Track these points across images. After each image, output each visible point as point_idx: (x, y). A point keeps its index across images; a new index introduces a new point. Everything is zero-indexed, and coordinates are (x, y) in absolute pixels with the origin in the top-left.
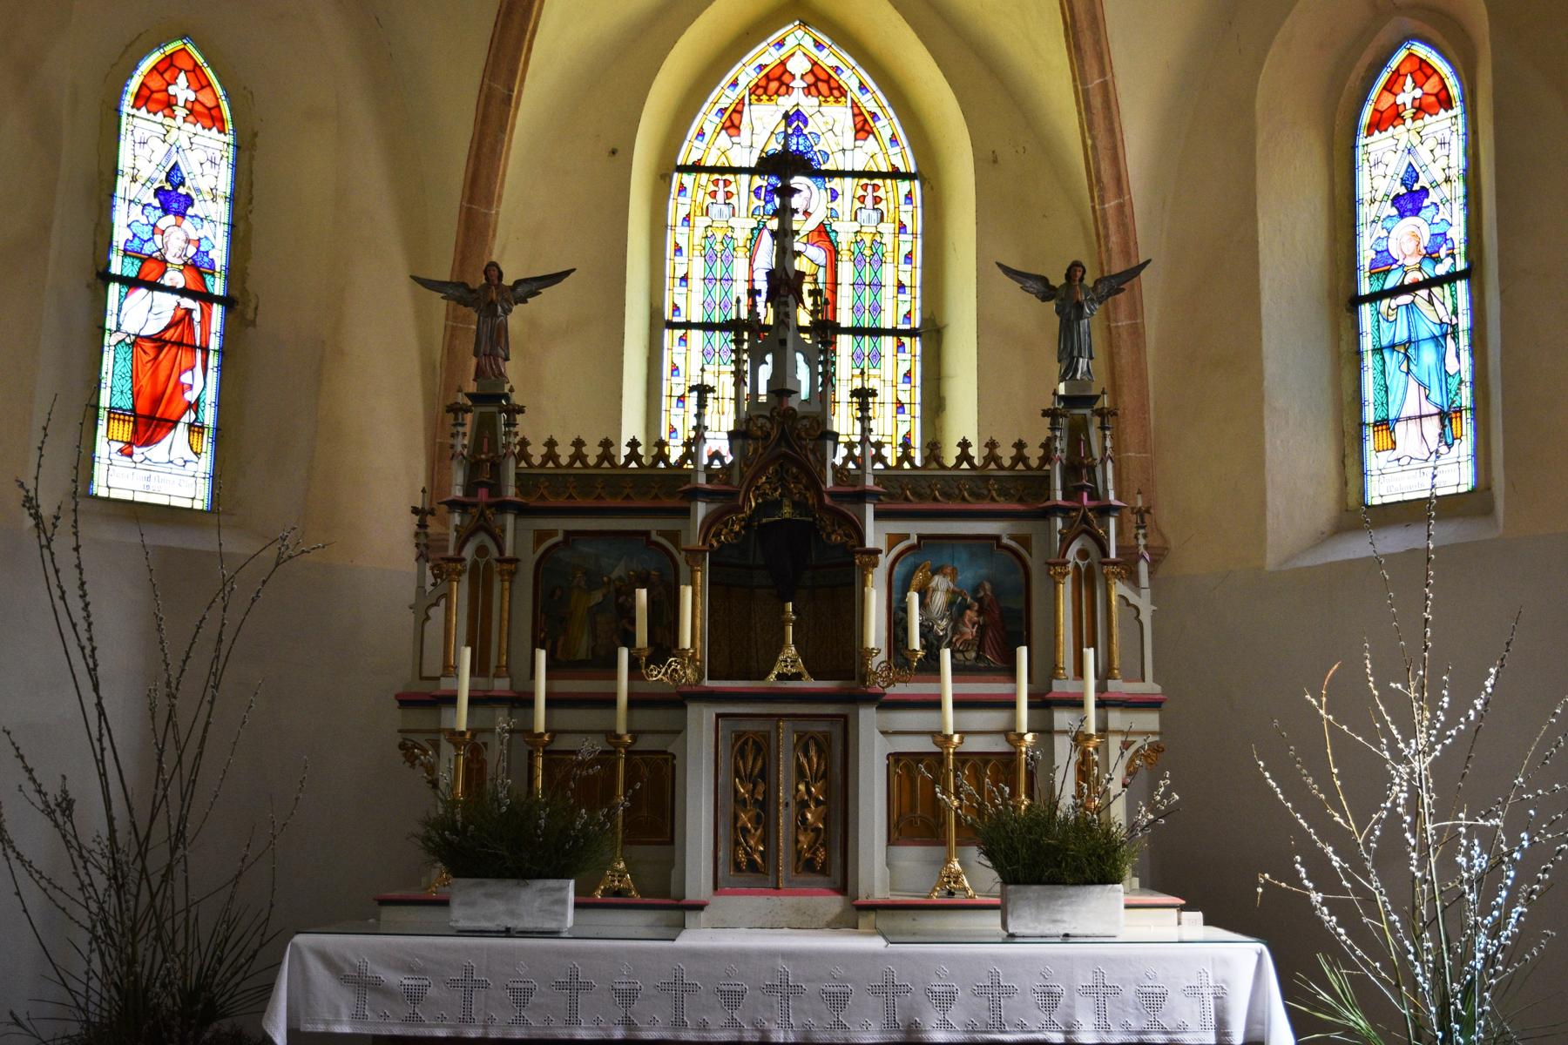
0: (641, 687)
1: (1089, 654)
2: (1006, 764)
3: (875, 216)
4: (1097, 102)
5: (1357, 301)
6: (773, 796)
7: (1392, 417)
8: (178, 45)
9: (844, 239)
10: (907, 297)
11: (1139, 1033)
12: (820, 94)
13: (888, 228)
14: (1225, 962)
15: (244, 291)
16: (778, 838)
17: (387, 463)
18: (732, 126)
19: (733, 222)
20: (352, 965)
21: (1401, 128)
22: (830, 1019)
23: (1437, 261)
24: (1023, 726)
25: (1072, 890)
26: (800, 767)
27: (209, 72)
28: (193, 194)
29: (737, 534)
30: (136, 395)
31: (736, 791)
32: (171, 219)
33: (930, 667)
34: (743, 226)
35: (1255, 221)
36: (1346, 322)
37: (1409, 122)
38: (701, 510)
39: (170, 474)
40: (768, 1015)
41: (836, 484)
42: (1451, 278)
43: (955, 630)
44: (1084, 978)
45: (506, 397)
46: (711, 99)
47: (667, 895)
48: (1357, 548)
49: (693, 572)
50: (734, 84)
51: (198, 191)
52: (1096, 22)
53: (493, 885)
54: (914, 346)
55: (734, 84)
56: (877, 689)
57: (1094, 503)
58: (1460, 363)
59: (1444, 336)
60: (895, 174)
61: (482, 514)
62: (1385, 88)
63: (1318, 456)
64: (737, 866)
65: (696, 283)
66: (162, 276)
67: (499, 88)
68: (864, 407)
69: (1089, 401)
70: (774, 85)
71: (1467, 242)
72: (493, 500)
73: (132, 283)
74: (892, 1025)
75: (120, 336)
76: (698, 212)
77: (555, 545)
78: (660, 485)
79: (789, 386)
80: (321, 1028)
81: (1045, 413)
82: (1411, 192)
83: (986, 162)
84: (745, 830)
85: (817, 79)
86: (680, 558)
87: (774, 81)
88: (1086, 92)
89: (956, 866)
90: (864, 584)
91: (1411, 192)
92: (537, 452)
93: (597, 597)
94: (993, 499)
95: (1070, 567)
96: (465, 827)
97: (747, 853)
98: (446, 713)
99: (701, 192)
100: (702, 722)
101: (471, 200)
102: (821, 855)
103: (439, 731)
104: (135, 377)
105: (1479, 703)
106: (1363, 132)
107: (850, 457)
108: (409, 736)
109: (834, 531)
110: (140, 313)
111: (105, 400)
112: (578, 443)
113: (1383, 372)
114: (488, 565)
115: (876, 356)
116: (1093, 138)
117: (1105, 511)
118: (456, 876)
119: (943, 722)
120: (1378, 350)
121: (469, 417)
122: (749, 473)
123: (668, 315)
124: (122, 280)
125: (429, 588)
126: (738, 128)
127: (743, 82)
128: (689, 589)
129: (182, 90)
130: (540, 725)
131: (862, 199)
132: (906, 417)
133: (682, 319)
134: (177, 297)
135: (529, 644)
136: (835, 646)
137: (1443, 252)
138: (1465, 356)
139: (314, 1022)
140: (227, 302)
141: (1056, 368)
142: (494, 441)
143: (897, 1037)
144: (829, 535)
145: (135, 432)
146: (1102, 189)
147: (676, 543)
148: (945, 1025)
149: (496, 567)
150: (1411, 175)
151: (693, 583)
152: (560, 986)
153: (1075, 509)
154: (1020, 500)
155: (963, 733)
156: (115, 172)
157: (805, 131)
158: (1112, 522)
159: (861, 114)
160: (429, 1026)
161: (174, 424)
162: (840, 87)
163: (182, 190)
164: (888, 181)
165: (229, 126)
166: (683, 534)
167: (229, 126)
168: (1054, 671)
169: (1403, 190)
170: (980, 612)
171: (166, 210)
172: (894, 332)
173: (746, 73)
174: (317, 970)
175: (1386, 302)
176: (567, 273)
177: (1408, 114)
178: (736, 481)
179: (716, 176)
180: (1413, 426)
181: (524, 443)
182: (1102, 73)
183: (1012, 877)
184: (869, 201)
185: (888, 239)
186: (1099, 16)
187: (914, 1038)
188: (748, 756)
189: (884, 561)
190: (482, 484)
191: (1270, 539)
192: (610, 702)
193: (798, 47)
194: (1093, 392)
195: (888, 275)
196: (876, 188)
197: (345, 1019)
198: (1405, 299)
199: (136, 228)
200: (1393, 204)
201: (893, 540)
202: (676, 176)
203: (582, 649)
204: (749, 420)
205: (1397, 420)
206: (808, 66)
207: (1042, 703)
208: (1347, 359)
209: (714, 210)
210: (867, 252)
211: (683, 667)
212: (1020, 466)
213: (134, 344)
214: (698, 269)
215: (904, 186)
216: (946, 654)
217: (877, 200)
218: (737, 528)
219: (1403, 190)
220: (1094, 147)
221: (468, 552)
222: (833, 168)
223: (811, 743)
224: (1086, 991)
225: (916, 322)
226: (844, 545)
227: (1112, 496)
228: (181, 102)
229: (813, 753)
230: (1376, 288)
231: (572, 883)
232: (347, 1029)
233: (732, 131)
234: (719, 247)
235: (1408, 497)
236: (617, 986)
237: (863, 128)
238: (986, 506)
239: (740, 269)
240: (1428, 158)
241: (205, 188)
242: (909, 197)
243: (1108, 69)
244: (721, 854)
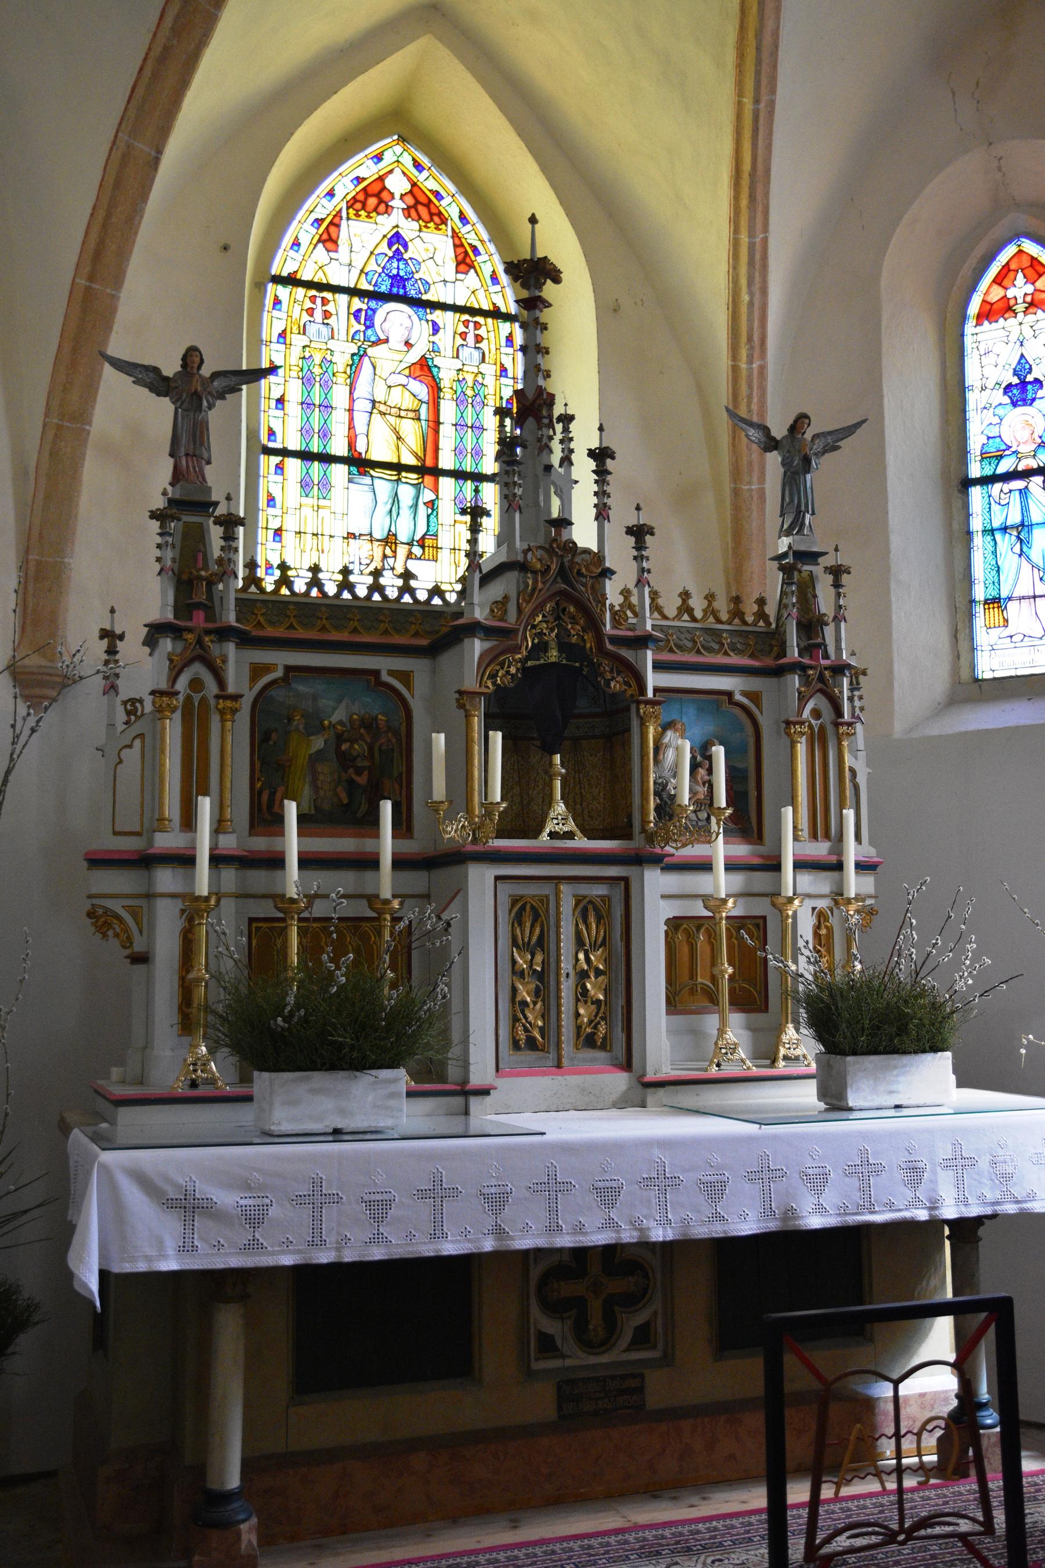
0: (410, 847)
1: (205, 805)
3: (477, 355)
5: (967, 483)
6: (553, 966)
7: (1004, 595)
9: (446, 377)
11: (994, 1204)
12: (420, 218)
13: (489, 370)
16: (559, 1013)
18: (329, 240)
19: (332, 344)
20: (177, 1186)
21: (1012, 321)
22: (708, 1211)
25: (906, 1059)
31: (514, 962)
35: (881, 398)
36: (957, 503)
37: (1020, 316)
38: (478, 646)
40: (645, 1211)
44: (944, 1151)
46: (306, 207)
53: (319, 1079)
55: (331, 194)
60: (496, 314)
61: (200, 642)
62: (994, 281)
64: (516, 1045)
65: (293, 407)
67: (142, 147)
68: (640, 546)
69: (812, 557)
72: (210, 626)
74: (768, 1212)
76: (295, 330)
80: (142, 1267)
84: (524, 1004)
85: (417, 202)
87: (371, 198)
93: (318, 743)
94: (726, 654)
97: (526, 1030)
99: (298, 308)
100: (481, 879)
101: (91, 278)
102: (602, 1029)
108: (96, 901)
109: (613, 678)
113: (995, 553)
119: (717, 887)
122: (528, 609)
125: (120, 727)
126: (335, 242)
127: (340, 193)
131: (463, 335)
133: (277, 445)
139: (133, 1260)
143: (772, 1226)
144: (608, 683)
148: (820, 1209)
150: (1022, 367)
152: (422, 1194)
153: (811, 667)
154: (752, 656)
157: (406, 256)
158: (846, 681)
159: (462, 245)
160: (273, 1253)
162: (440, 214)
164: (490, 320)
169: (1015, 381)
173: (342, 183)
174: (133, 1195)
175: (998, 486)
177: (1020, 308)
184: (471, 339)
185: (490, 381)
187: (791, 1225)
188: (528, 922)
191: (897, 708)
192: (372, 863)
193: (396, 164)
197: (171, 1252)
200: (1005, 393)
205: (1010, 599)
206: (408, 187)
208: (960, 538)
209: (312, 329)
210: (470, 393)
214: (295, 392)
215: (505, 328)
217: (479, 339)
218: (513, 670)
219: (1015, 381)
221: (182, 684)
222: (434, 299)
223: (590, 907)
224: (948, 1164)
230: (988, 471)
232: (170, 1264)
233: (329, 245)
234: (317, 371)
235: (1020, 672)
236: (486, 1191)
237: (465, 262)
238: (720, 659)
242: (510, 339)
244: (500, 1032)
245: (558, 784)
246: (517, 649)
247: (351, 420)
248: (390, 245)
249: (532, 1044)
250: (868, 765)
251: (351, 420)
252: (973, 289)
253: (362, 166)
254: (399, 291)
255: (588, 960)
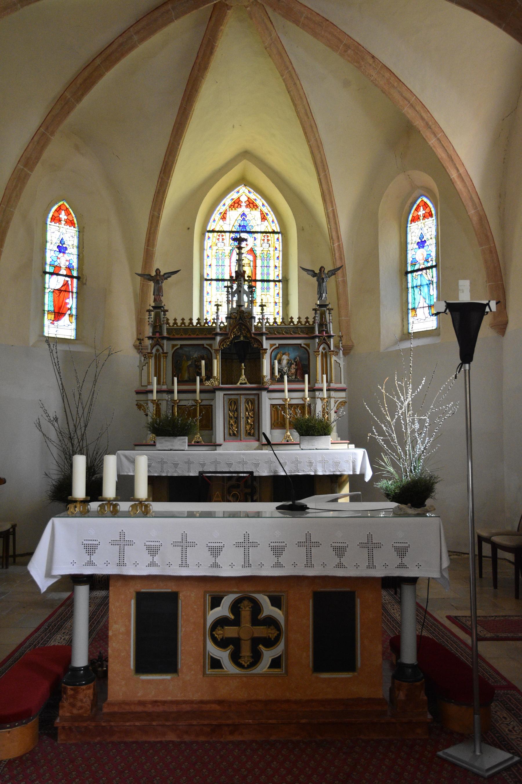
0: (203, 387)
2: (303, 406)
3: (268, 245)
4: (331, 215)
5: (407, 273)
8: (61, 203)
9: (258, 253)
10: (277, 270)
13: (272, 249)
14: (355, 454)
15: (82, 274)
17: (125, 329)
18: (224, 218)
19: (224, 248)
21: (419, 222)
23: (428, 262)
24: (307, 396)
25: (317, 437)
26: (246, 408)
27: (70, 210)
28: (67, 247)
29: (228, 345)
30: (54, 307)
31: (229, 415)
32: (62, 254)
33: (281, 380)
34: (228, 249)
36: (404, 280)
37: (421, 220)
38: (218, 338)
39: (65, 329)
41: (255, 331)
42: (431, 267)
43: (289, 370)
44: (319, 459)
45: (163, 308)
47: (211, 442)
48: (406, 345)
49: (216, 355)
50: (224, 205)
51: (68, 245)
52: (330, 192)
53: (167, 438)
54: (280, 285)
55: (224, 205)
56: (267, 386)
57: (327, 335)
58: (434, 292)
59: (430, 284)
60: (274, 232)
61: (158, 340)
63: (397, 318)
64: (230, 435)
65: (213, 266)
66: (60, 271)
67: (156, 214)
69: (325, 306)
70: (236, 205)
71: (436, 257)
73: (52, 274)
75: (49, 290)
77: (178, 348)
78: (205, 331)
79: (242, 304)
80: (125, 474)
81: (313, 310)
82: (422, 241)
83: (301, 230)
84: (232, 425)
85: (250, 203)
86: (213, 352)
87: (236, 204)
88: (328, 213)
89: (289, 434)
90: (263, 358)
91: (422, 241)
92: (171, 322)
95: (320, 352)
96: (159, 423)
98: (150, 395)
100: (220, 396)
101: (148, 246)
102: (252, 431)
103: (148, 400)
104: (54, 301)
105: (420, 387)
106: (409, 222)
107: (259, 322)
110: (54, 283)
111: (46, 308)
112: (183, 319)
114: (159, 354)
115: (268, 288)
116: (330, 226)
117: (330, 337)
118: (157, 436)
119: (285, 396)
120: (413, 287)
121: (153, 313)
123: (205, 277)
124: (50, 273)
125: (143, 361)
128: (216, 360)
129: (63, 216)
130: (176, 398)
132: (278, 307)
133: (209, 278)
134: (64, 277)
135: (171, 375)
136: (255, 376)
137: (430, 260)
138: (435, 289)
139: (123, 472)
140: (78, 278)
141: (317, 296)
142: (160, 319)
143: (272, 474)
145: (55, 317)
146: (333, 240)
147: (211, 348)
149: (162, 355)
150: (422, 237)
151: (216, 358)
153: (321, 336)
154: (307, 334)
155: (291, 399)
156: (46, 242)
161: (65, 314)
162: (256, 205)
163: (64, 246)
164: (272, 234)
165: (76, 226)
166: (213, 345)
167: (76, 226)
168: (316, 381)
170: (296, 365)
171: (60, 252)
172: (274, 281)
173: (228, 201)
174: (124, 459)
175: (415, 273)
176: (178, 271)
177: (421, 218)
178: (228, 330)
179: (219, 234)
180: (422, 309)
181: (168, 320)
182: (332, 207)
183: (301, 435)
184: (266, 241)
185: (272, 252)
186: (331, 191)
187: (276, 474)
188: (233, 405)
189: (269, 352)
190: (157, 332)
191: (381, 343)
192: (194, 391)
193: (243, 193)
194: (327, 303)
195: (272, 264)
196: (268, 236)
198: (420, 273)
199: (53, 258)
201: (272, 345)
202: (207, 234)
203: (186, 377)
204: (231, 314)
206: (247, 199)
207: (312, 390)
209: (219, 244)
210: (265, 256)
211: (215, 381)
212: (307, 324)
213: (53, 292)
215: (276, 236)
216: (286, 377)
217: (268, 240)
218: (228, 343)
219: (420, 241)
220: (330, 228)
221: (154, 351)
225: (280, 278)
226: (257, 347)
227: (332, 332)
228: (63, 220)
229: (250, 404)
231: (187, 438)
238: (297, 336)
239: (227, 262)
240: (426, 231)
241: (71, 245)
242: (278, 239)
243: (334, 205)
245: (243, 371)
246: (229, 338)
247: (230, 268)
248: (241, 216)
249: (234, 435)
250: (344, 361)
251: (230, 268)
252: (410, 213)
253: (233, 195)
254: (243, 229)
255: (249, 414)
